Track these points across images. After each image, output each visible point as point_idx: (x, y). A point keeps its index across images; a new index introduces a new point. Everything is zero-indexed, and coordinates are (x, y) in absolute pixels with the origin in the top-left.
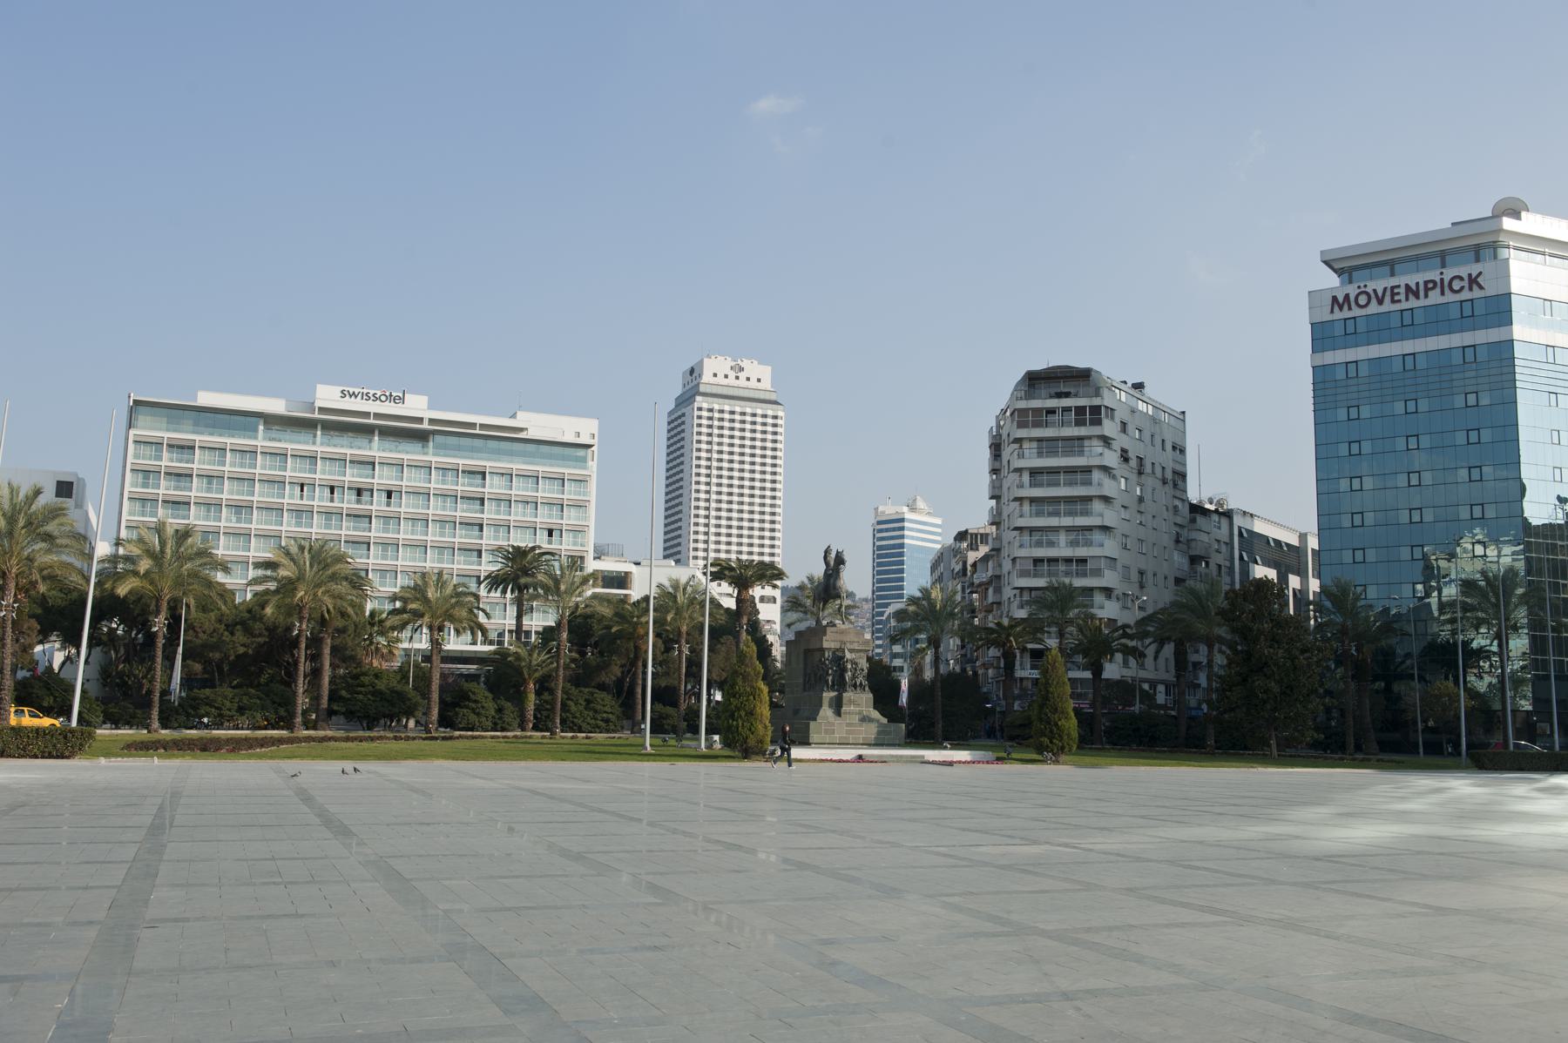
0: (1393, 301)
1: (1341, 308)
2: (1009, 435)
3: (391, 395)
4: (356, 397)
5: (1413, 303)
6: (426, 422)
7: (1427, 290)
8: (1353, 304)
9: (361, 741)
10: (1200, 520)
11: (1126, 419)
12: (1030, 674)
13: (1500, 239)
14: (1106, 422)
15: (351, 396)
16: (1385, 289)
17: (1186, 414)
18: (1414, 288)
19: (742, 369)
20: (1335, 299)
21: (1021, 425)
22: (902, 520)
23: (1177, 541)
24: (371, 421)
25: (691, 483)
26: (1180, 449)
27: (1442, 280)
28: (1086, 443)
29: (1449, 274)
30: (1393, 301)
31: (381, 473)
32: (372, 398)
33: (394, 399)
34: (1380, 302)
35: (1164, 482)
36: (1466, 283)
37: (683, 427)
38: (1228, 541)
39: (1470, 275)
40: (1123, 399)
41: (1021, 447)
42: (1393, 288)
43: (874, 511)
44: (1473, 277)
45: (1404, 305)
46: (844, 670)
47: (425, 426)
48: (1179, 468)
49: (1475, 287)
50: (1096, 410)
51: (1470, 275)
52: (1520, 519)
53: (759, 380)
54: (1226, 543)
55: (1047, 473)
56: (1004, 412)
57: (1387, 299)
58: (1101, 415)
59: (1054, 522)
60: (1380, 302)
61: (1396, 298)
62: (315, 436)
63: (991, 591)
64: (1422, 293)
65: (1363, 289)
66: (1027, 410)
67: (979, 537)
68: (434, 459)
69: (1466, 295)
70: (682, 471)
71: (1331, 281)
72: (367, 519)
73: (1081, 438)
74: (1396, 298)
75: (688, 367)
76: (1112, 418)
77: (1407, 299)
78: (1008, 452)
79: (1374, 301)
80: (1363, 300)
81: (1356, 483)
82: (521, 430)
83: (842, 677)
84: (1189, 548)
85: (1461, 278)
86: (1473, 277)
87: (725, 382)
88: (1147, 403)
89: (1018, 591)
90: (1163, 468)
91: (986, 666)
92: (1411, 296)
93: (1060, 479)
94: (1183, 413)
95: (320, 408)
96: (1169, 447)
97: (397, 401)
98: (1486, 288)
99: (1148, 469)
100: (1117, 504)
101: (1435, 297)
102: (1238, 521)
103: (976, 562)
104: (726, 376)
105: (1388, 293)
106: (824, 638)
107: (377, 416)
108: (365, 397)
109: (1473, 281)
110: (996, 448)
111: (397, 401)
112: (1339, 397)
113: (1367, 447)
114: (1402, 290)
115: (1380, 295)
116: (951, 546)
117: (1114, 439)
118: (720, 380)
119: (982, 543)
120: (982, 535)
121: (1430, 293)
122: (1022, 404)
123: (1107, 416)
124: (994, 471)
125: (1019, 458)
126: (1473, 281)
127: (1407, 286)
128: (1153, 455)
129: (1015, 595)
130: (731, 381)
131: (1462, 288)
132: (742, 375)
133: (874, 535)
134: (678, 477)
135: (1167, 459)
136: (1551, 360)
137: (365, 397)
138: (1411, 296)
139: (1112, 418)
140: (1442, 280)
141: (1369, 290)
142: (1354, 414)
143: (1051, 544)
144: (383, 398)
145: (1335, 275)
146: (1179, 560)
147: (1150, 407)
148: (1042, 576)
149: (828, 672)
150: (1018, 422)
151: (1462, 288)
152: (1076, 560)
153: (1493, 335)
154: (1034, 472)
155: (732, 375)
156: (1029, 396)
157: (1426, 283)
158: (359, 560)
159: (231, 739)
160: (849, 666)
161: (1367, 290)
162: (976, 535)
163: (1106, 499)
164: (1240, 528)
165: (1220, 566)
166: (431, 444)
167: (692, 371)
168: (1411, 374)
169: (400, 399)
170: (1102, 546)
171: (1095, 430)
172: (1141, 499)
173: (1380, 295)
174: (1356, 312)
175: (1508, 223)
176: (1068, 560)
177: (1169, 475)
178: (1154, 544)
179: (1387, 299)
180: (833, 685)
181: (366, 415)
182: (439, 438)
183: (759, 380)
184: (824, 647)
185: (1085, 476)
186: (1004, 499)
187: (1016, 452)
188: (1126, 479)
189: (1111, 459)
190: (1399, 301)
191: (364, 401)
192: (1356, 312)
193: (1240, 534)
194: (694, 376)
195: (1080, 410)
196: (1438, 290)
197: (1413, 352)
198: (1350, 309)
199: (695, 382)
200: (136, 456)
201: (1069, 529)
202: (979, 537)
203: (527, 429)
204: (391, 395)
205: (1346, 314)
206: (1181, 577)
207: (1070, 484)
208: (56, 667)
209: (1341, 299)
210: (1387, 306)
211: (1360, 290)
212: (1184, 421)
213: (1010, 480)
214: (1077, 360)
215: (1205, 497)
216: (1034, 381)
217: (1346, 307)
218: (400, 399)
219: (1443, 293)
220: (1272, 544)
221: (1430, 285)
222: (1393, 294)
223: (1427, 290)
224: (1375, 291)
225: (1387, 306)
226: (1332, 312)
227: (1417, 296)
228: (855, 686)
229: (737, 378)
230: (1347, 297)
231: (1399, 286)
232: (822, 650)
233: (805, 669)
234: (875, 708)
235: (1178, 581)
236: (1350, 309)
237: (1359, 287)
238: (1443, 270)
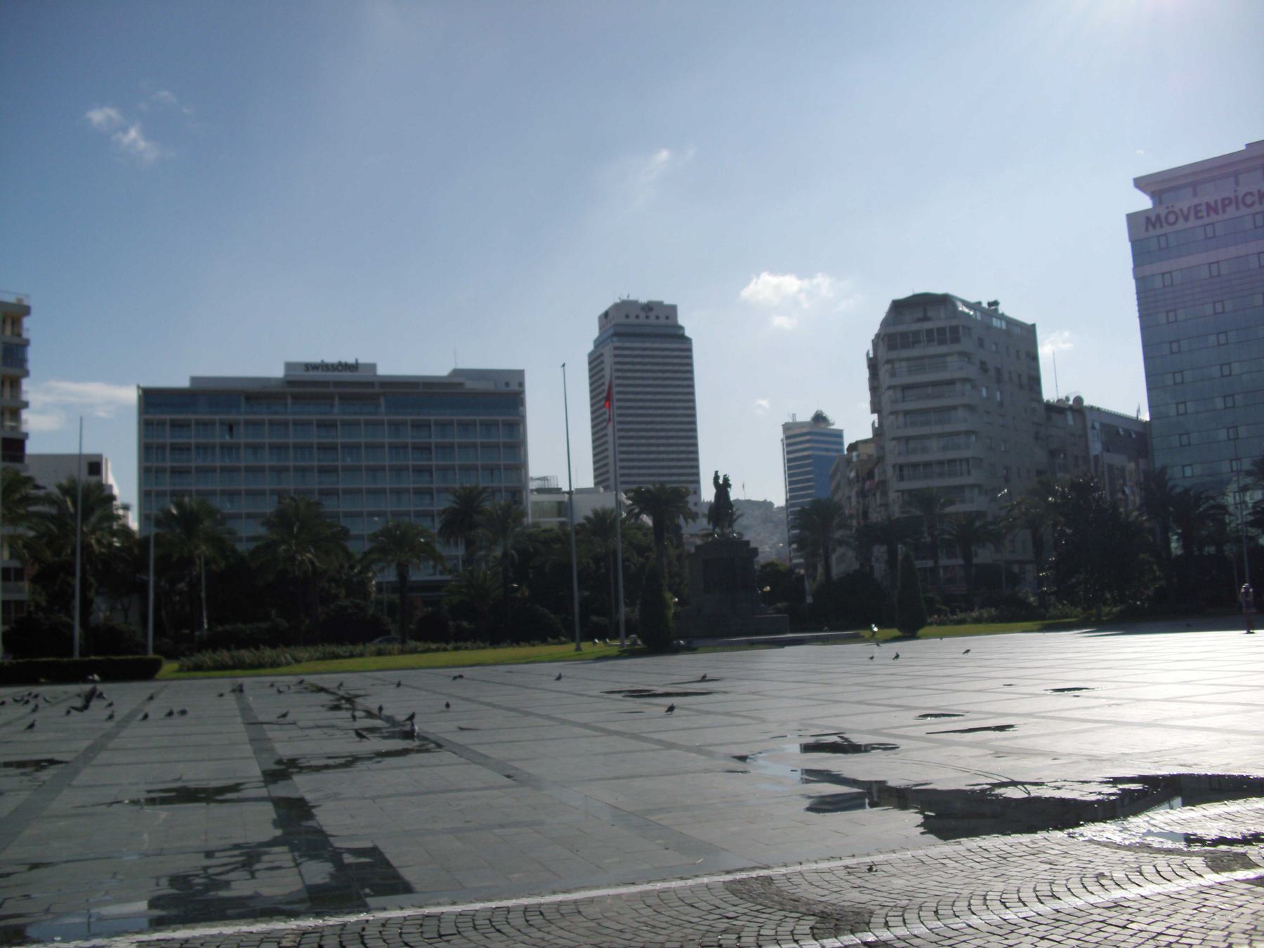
0: (1197, 218)
1: (1154, 226)
5: (1213, 218)
7: (1224, 206)
9: (997, 738)
10: (1055, 416)
20: (1148, 219)
23: (1037, 437)
24: (332, 390)
27: (1236, 197)
28: (949, 359)
29: (1242, 191)
30: (1197, 218)
34: (1186, 219)
35: (1021, 386)
36: (1256, 198)
42: (1196, 206)
45: (1206, 220)
57: (1192, 217)
59: (925, 430)
61: (1200, 215)
62: (286, 405)
63: (878, 494)
64: (1220, 210)
65: (1171, 209)
68: (386, 418)
73: (944, 356)
74: (1200, 215)
75: (558, 682)
87: (637, 321)
92: (1212, 213)
101: (1231, 210)
105: (1192, 212)
108: (325, 368)
114: (1203, 208)
118: (632, 320)
122: (892, 330)
130: (642, 320)
132: (652, 315)
138: (1212, 213)
140: (1236, 197)
141: (1176, 209)
142: (1171, 315)
143: (925, 450)
154: (905, 388)
155: (642, 315)
157: (1223, 200)
158: (330, 505)
165: (1076, 457)
171: (957, 347)
172: (1001, 404)
176: (941, 463)
177: (1025, 380)
179: (1192, 217)
183: (667, 318)
188: (987, 388)
189: (972, 371)
190: (1202, 217)
194: (609, 318)
197: (1216, 260)
201: (940, 436)
205: (1159, 231)
208: (1019, 333)
209: (1153, 219)
210: (1192, 222)
217: (1158, 226)
219: (1237, 208)
221: (1227, 202)
222: (1197, 212)
223: (1224, 206)
225: (1192, 222)
226: (1147, 230)
227: (1216, 212)
229: (647, 317)
230: (1158, 217)
231: (1200, 205)
235: (1039, 473)
236: (1161, 226)
237: (1167, 208)
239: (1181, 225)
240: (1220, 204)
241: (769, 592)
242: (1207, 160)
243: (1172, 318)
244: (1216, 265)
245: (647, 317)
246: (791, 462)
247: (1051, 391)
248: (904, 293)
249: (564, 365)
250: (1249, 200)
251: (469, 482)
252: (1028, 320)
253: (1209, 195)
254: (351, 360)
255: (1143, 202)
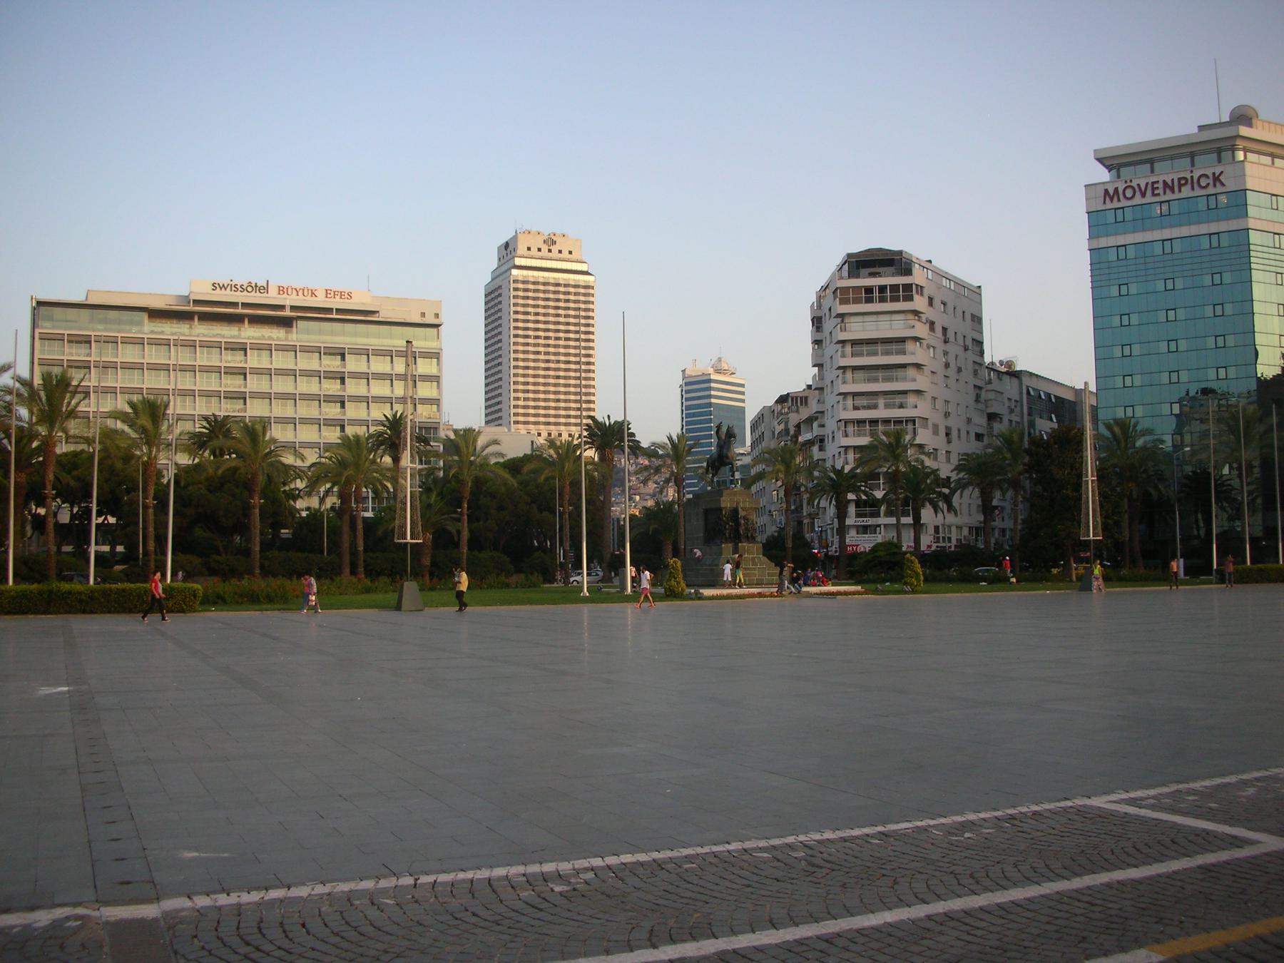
0: (1154, 195)
1: (1112, 200)
2: (830, 309)
3: (256, 286)
4: (226, 289)
5: (1169, 196)
6: (288, 309)
7: (1180, 186)
8: (1121, 196)
11: (932, 295)
12: (855, 522)
13: (1237, 143)
14: (916, 297)
15: (221, 289)
16: (1147, 184)
17: (982, 288)
18: (1170, 183)
19: (554, 243)
20: (1106, 191)
21: (844, 301)
22: (710, 381)
24: (240, 311)
25: (510, 352)
26: (977, 320)
27: (1192, 177)
30: (1154, 195)
31: (202, 356)
32: (240, 289)
33: (259, 289)
34: (1143, 195)
37: (500, 299)
38: (1018, 400)
39: (1214, 174)
40: (952, 288)
41: (842, 321)
42: (1153, 183)
43: (681, 373)
44: (1217, 175)
46: (738, 524)
47: (288, 313)
48: (976, 336)
49: (1218, 184)
50: (908, 287)
51: (1214, 174)
52: (1255, 378)
53: (570, 253)
54: (1016, 401)
55: (867, 343)
56: (825, 288)
57: (1149, 193)
58: (912, 291)
60: (1143, 195)
61: (1156, 192)
64: (1176, 189)
65: (1129, 184)
66: (848, 288)
67: (799, 399)
69: (1211, 190)
70: (500, 341)
71: (1103, 175)
72: (242, 401)
74: (1156, 192)
76: (922, 295)
77: (1165, 193)
78: (828, 325)
79: (1138, 194)
80: (1129, 193)
81: (1127, 352)
82: (373, 312)
83: (739, 532)
84: (987, 407)
85: (1206, 176)
86: (1217, 175)
88: (927, 269)
89: (843, 449)
90: (964, 337)
91: (813, 516)
92: (1168, 191)
93: (878, 350)
94: (980, 287)
95: (194, 301)
96: (968, 317)
97: (262, 291)
98: (1226, 184)
99: (952, 339)
100: (927, 370)
101: (1186, 191)
102: (1026, 381)
103: (800, 423)
104: (539, 250)
105: (1149, 187)
106: (722, 499)
107: (245, 305)
108: (233, 289)
109: (1216, 179)
110: (817, 322)
111: (262, 291)
112: (1112, 276)
113: (1135, 319)
114: (1160, 185)
115: (1143, 189)
116: (771, 407)
117: (922, 313)
119: (801, 404)
120: (801, 398)
121: (1183, 189)
123: (917, 293)
124: (817, 342)
125: (841, 331)
126: (1216, 179)
127: (1164, 181)
128: (954, 324)
129: (840, 452)
131: (1208, 184)
132: (555, 249)
133: (682, 396)
134: (496, 346)
135: (966, 328)
136: (1277, 246)
137: (233, 289)
138: (1168, 191)
139: (922, 295)
140: (1192, 177)
141: (1134, 184)
144: (250, 289)
145: (1107, 171)
146: (981, 421)
147: (952, 283)
148: (865, 435)
149: (725, 527)
150: (840, 299)
151: (1208, 184)
152: (894, 422)
153: (1234, 225)
155: (545, 248)
156: (853, 274)
157: (1179, 179)
159: (1105, 517)
160: (743, 522)
161: (1132, 184)
162: (797, 398)
163: (918, 366)
164: (1027, 387)
166: (294, 329)
167: (507, 245)
168: (1169, 257)
169: (265, 289)
170: (916, 407)
173: (1143, 189)
174: (1124, 203)
175: (1244, 131)
177: (969, 342)
178: (967, 407)
179: (1149, 193)
180: (730, 537)
181: (234, 305)
182: (301, 324)
184: (722, 506)
185: (900, 346)
186: (827, 366)
187: (839, 326)
190: (1158, 194)
191: (233, 293)
192: (1124, 203)
193: (1028, 393)
194: (509, 250)
195: (895, 288)
196: (1189, 186)
198: (1119, 200)
199: (510, 256)
200: (42, 351)
202: (799, 399)
203: (378, 312)
204: (256, 286)
205: (1116, 204)
206: (980, 432)
207: (887, 353)
209: (1111, 192)
210: (1149, 198)
211: (1126, 185)
212: (980, 295)
213: (830, 349)
214: (890, 243)
215: (996, 360)
216: (862, 263)
217: (1115, 199)
218: (265, 289)
220: (1053, 400)
221: (1183, 182)
222: (1153, 189)
223: (1180, 186)
224: (1139, 185)
225: (1149, 198)
226: (1104, 202)
228: (747, 537)
229: (550, 251)
230: (1116, 190)
232: (720, 509)
233: (706, 524)
234: (764, 555)
236: (1119, 200)
238: (1192, 169)
239: (1138, 200)
240: (1176, 183)
241: (61, 499)
242: (1165, 139)
243: (1219, 310)
244: (1280, 275)
245: (550, 251)
246: (688, 401)
247: (994, 353)
248: (858, 247)
249: (832, 357)
250: (1203, 182)
251: (152, 382)
252: (972, 280)
253: (1166, 173)
254: (262, 283)
255: (1102, 175)
